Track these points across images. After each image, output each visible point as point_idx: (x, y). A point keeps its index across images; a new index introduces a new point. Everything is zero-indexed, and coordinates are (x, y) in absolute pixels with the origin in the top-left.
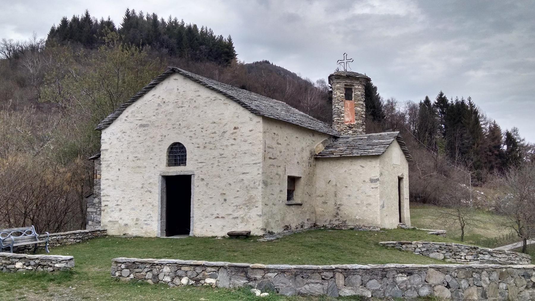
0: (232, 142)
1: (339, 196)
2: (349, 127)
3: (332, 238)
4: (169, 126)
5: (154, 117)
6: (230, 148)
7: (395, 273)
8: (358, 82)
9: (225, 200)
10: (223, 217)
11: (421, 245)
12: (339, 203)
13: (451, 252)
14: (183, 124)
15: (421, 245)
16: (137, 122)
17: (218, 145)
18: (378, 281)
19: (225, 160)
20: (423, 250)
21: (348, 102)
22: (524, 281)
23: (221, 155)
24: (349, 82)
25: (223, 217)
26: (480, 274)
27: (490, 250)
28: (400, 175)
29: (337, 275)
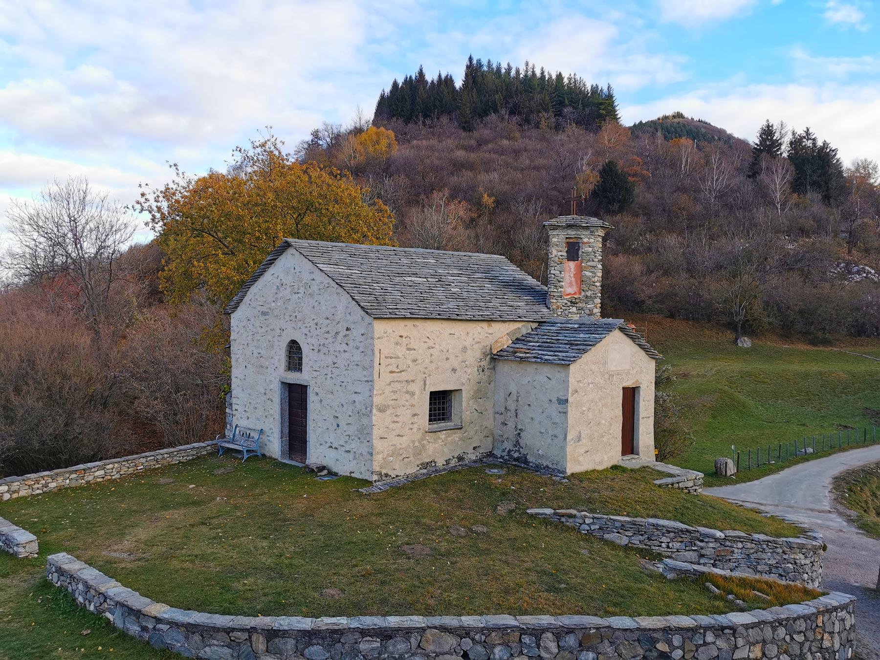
0: (344, 347)
1: (520, 416)
2: (571, 302)
3: (99, 655)
4: (287, 318)
5: (273, 304)
6: (343, 354)
7: (357, 635)
8: (588, 233)
9: (338, 426)
10: (336, 448)
11: (591, 520)
12: (519, 427)
13: (642, 535)
14: (299, 316)
15: (591, 520)
16: (259, 308)
17: (331, 349)
18: (324, 648)
19: (337, 372)
20: (593, 527)
21: (572, 264)
22: (639, 648)
23: (334, 364)
24: (572, 233)
25: (336, 448)
26: (538, 639)
27: (719, 534)
28: (629, 384)
29: (254, 637)
